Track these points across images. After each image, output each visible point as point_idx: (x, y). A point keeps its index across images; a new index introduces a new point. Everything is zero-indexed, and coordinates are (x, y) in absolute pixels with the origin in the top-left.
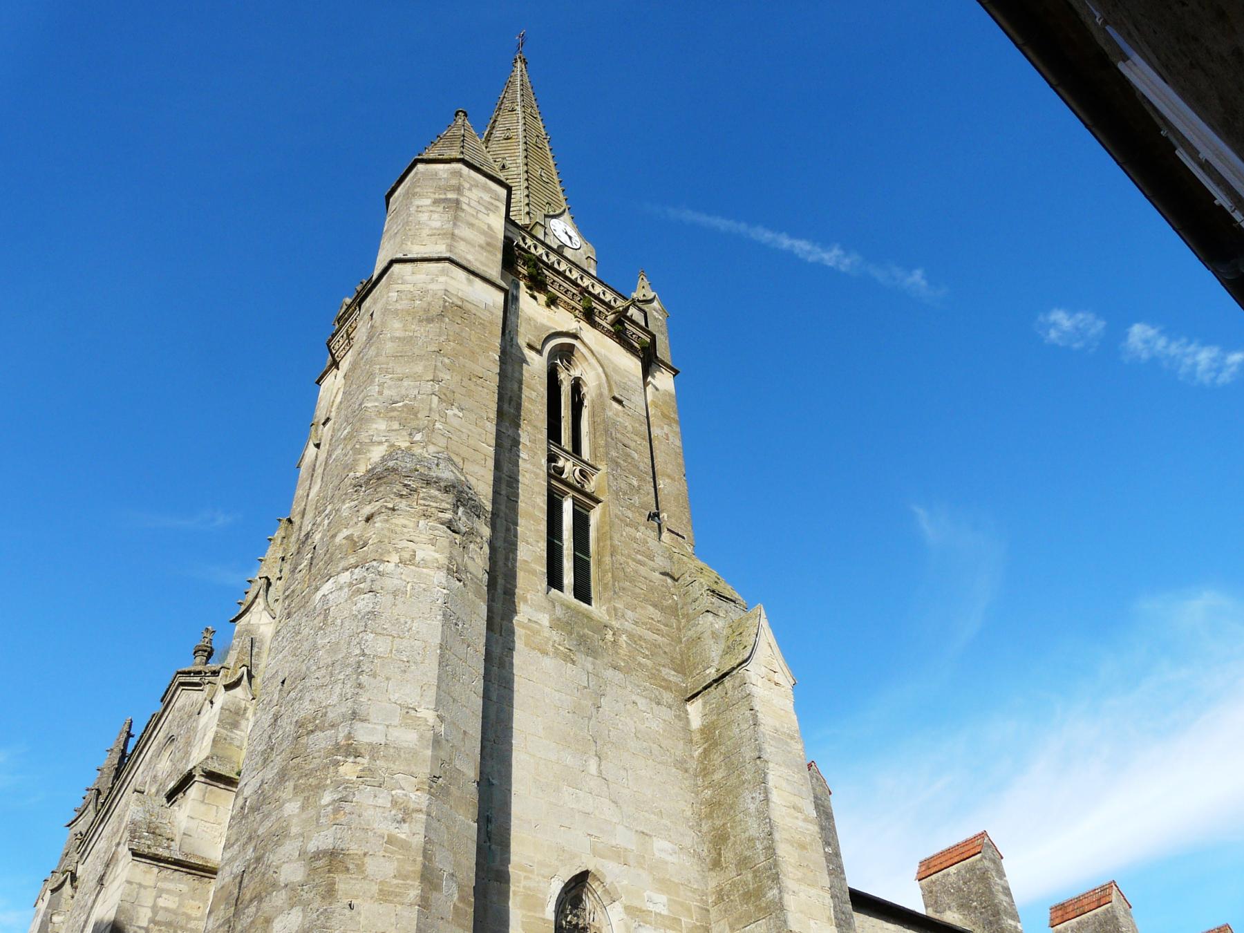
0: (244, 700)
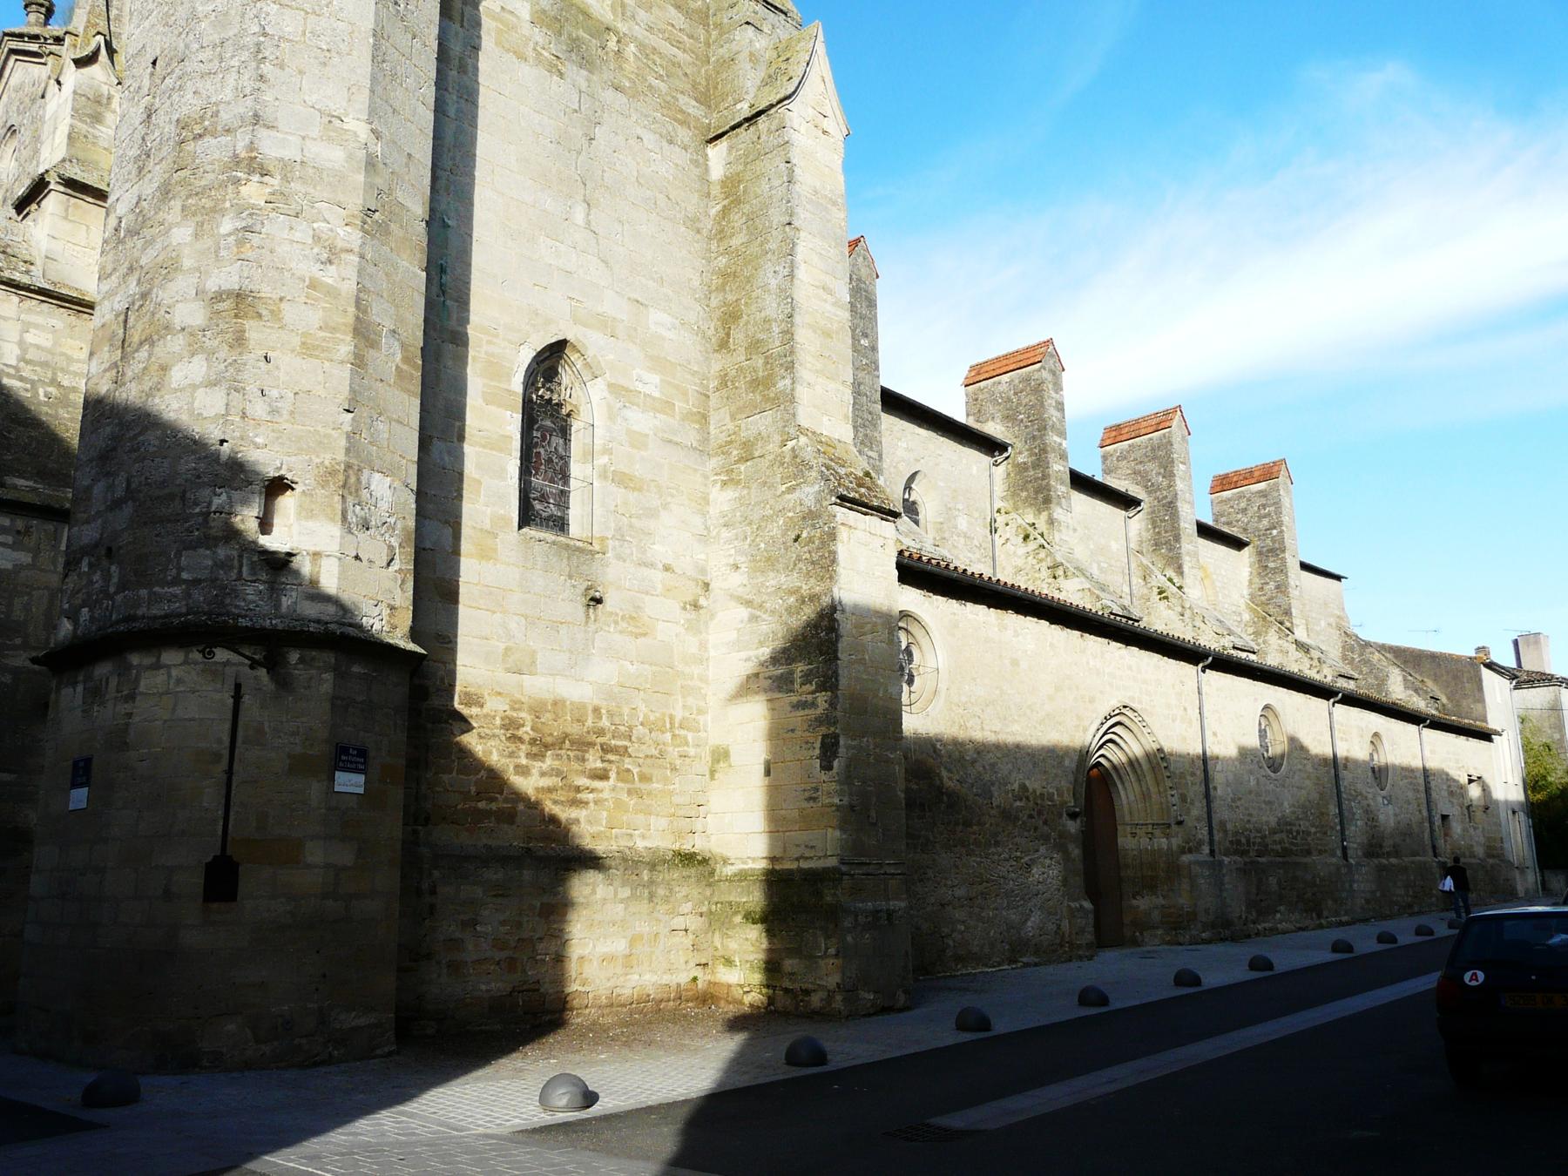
0: (106, 84)
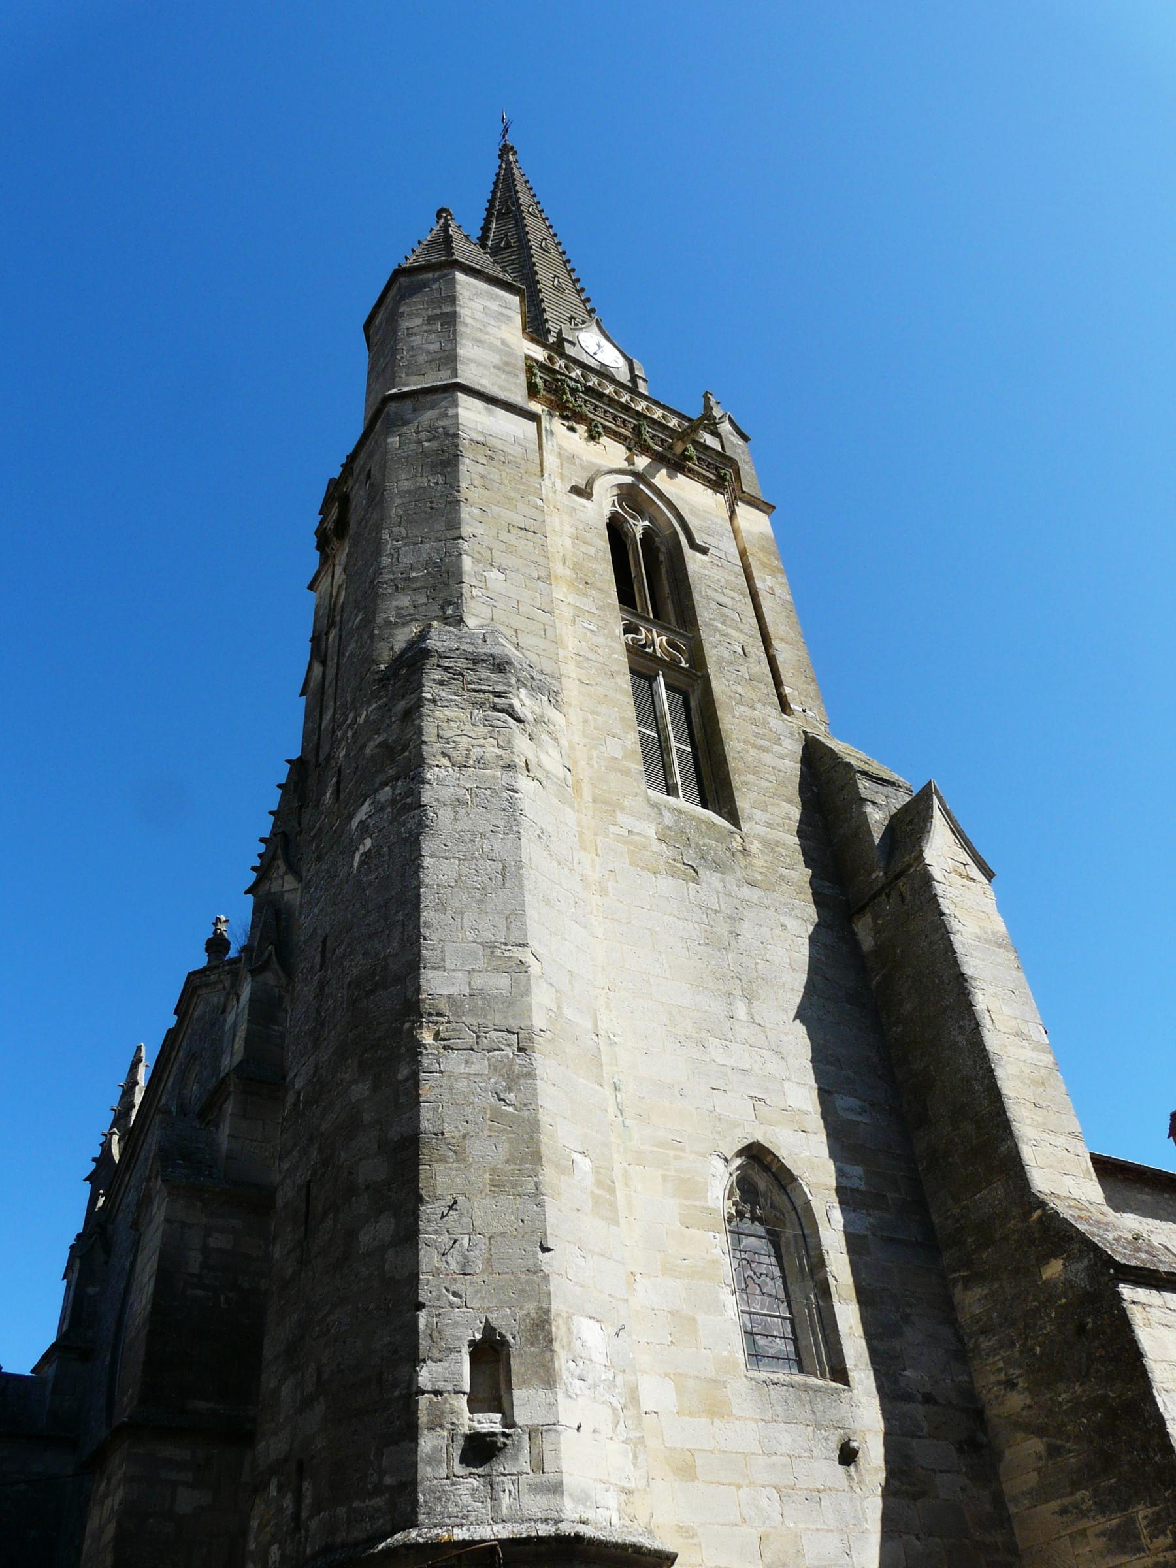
0: (276, 986)
